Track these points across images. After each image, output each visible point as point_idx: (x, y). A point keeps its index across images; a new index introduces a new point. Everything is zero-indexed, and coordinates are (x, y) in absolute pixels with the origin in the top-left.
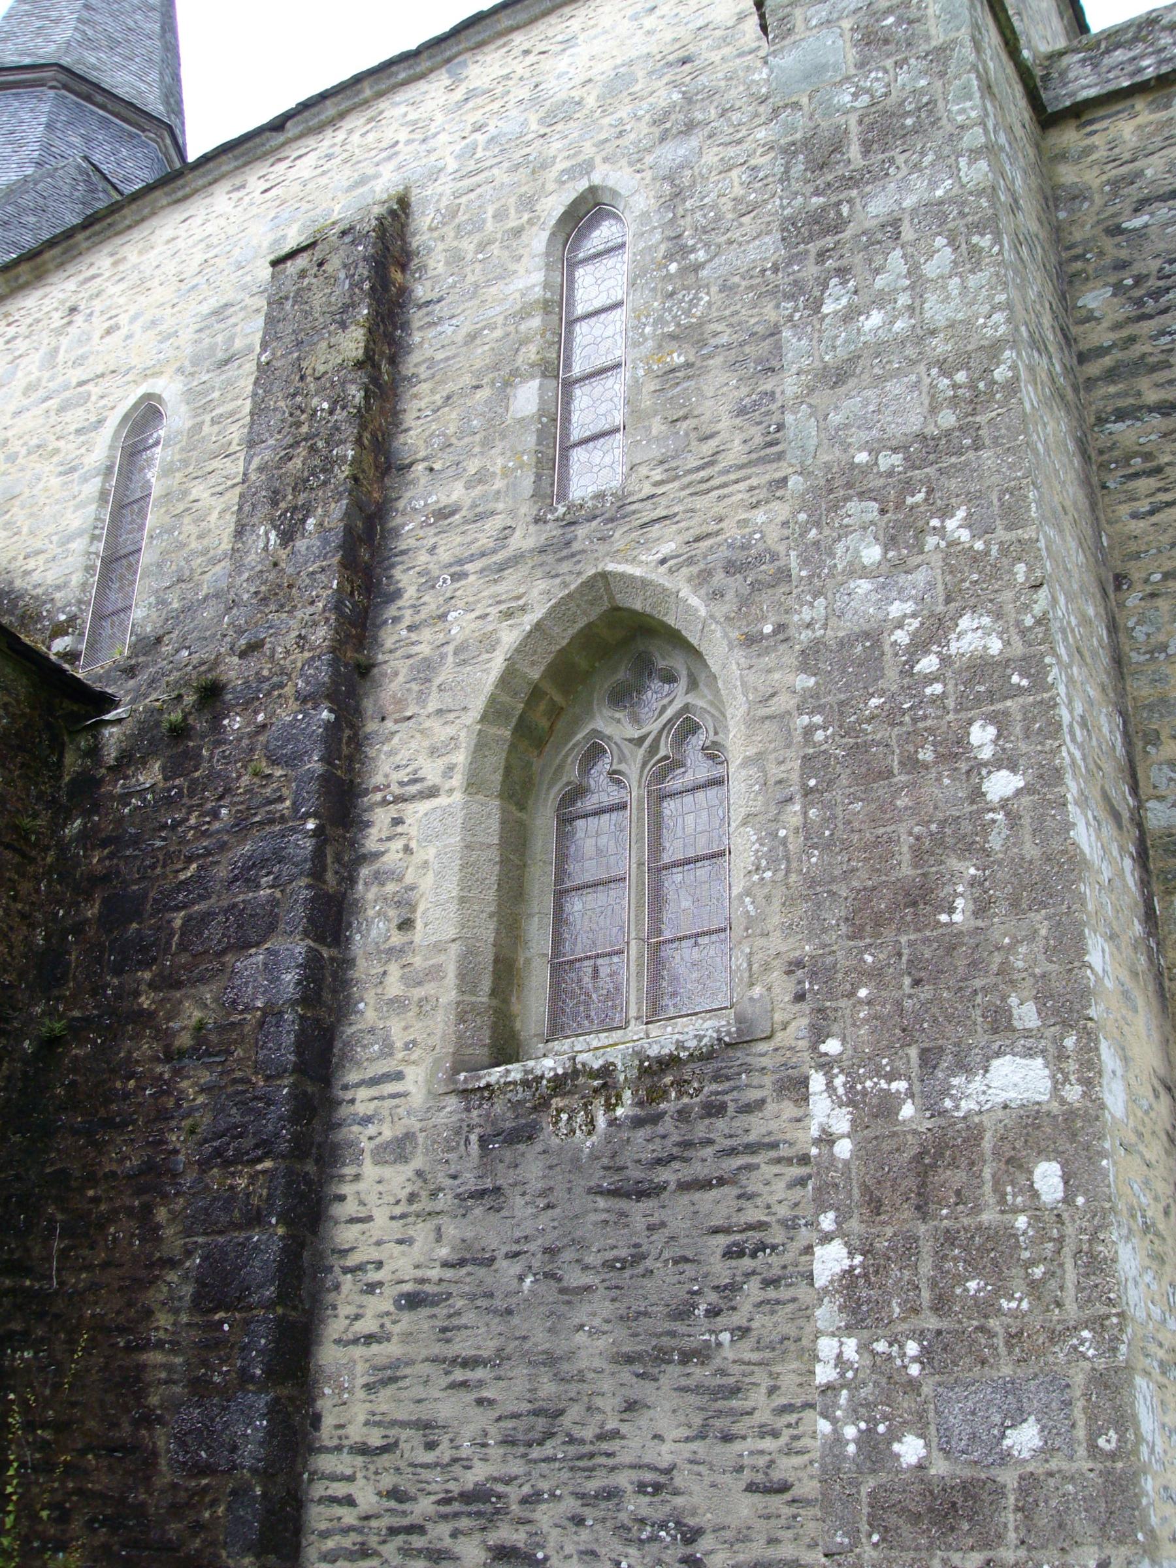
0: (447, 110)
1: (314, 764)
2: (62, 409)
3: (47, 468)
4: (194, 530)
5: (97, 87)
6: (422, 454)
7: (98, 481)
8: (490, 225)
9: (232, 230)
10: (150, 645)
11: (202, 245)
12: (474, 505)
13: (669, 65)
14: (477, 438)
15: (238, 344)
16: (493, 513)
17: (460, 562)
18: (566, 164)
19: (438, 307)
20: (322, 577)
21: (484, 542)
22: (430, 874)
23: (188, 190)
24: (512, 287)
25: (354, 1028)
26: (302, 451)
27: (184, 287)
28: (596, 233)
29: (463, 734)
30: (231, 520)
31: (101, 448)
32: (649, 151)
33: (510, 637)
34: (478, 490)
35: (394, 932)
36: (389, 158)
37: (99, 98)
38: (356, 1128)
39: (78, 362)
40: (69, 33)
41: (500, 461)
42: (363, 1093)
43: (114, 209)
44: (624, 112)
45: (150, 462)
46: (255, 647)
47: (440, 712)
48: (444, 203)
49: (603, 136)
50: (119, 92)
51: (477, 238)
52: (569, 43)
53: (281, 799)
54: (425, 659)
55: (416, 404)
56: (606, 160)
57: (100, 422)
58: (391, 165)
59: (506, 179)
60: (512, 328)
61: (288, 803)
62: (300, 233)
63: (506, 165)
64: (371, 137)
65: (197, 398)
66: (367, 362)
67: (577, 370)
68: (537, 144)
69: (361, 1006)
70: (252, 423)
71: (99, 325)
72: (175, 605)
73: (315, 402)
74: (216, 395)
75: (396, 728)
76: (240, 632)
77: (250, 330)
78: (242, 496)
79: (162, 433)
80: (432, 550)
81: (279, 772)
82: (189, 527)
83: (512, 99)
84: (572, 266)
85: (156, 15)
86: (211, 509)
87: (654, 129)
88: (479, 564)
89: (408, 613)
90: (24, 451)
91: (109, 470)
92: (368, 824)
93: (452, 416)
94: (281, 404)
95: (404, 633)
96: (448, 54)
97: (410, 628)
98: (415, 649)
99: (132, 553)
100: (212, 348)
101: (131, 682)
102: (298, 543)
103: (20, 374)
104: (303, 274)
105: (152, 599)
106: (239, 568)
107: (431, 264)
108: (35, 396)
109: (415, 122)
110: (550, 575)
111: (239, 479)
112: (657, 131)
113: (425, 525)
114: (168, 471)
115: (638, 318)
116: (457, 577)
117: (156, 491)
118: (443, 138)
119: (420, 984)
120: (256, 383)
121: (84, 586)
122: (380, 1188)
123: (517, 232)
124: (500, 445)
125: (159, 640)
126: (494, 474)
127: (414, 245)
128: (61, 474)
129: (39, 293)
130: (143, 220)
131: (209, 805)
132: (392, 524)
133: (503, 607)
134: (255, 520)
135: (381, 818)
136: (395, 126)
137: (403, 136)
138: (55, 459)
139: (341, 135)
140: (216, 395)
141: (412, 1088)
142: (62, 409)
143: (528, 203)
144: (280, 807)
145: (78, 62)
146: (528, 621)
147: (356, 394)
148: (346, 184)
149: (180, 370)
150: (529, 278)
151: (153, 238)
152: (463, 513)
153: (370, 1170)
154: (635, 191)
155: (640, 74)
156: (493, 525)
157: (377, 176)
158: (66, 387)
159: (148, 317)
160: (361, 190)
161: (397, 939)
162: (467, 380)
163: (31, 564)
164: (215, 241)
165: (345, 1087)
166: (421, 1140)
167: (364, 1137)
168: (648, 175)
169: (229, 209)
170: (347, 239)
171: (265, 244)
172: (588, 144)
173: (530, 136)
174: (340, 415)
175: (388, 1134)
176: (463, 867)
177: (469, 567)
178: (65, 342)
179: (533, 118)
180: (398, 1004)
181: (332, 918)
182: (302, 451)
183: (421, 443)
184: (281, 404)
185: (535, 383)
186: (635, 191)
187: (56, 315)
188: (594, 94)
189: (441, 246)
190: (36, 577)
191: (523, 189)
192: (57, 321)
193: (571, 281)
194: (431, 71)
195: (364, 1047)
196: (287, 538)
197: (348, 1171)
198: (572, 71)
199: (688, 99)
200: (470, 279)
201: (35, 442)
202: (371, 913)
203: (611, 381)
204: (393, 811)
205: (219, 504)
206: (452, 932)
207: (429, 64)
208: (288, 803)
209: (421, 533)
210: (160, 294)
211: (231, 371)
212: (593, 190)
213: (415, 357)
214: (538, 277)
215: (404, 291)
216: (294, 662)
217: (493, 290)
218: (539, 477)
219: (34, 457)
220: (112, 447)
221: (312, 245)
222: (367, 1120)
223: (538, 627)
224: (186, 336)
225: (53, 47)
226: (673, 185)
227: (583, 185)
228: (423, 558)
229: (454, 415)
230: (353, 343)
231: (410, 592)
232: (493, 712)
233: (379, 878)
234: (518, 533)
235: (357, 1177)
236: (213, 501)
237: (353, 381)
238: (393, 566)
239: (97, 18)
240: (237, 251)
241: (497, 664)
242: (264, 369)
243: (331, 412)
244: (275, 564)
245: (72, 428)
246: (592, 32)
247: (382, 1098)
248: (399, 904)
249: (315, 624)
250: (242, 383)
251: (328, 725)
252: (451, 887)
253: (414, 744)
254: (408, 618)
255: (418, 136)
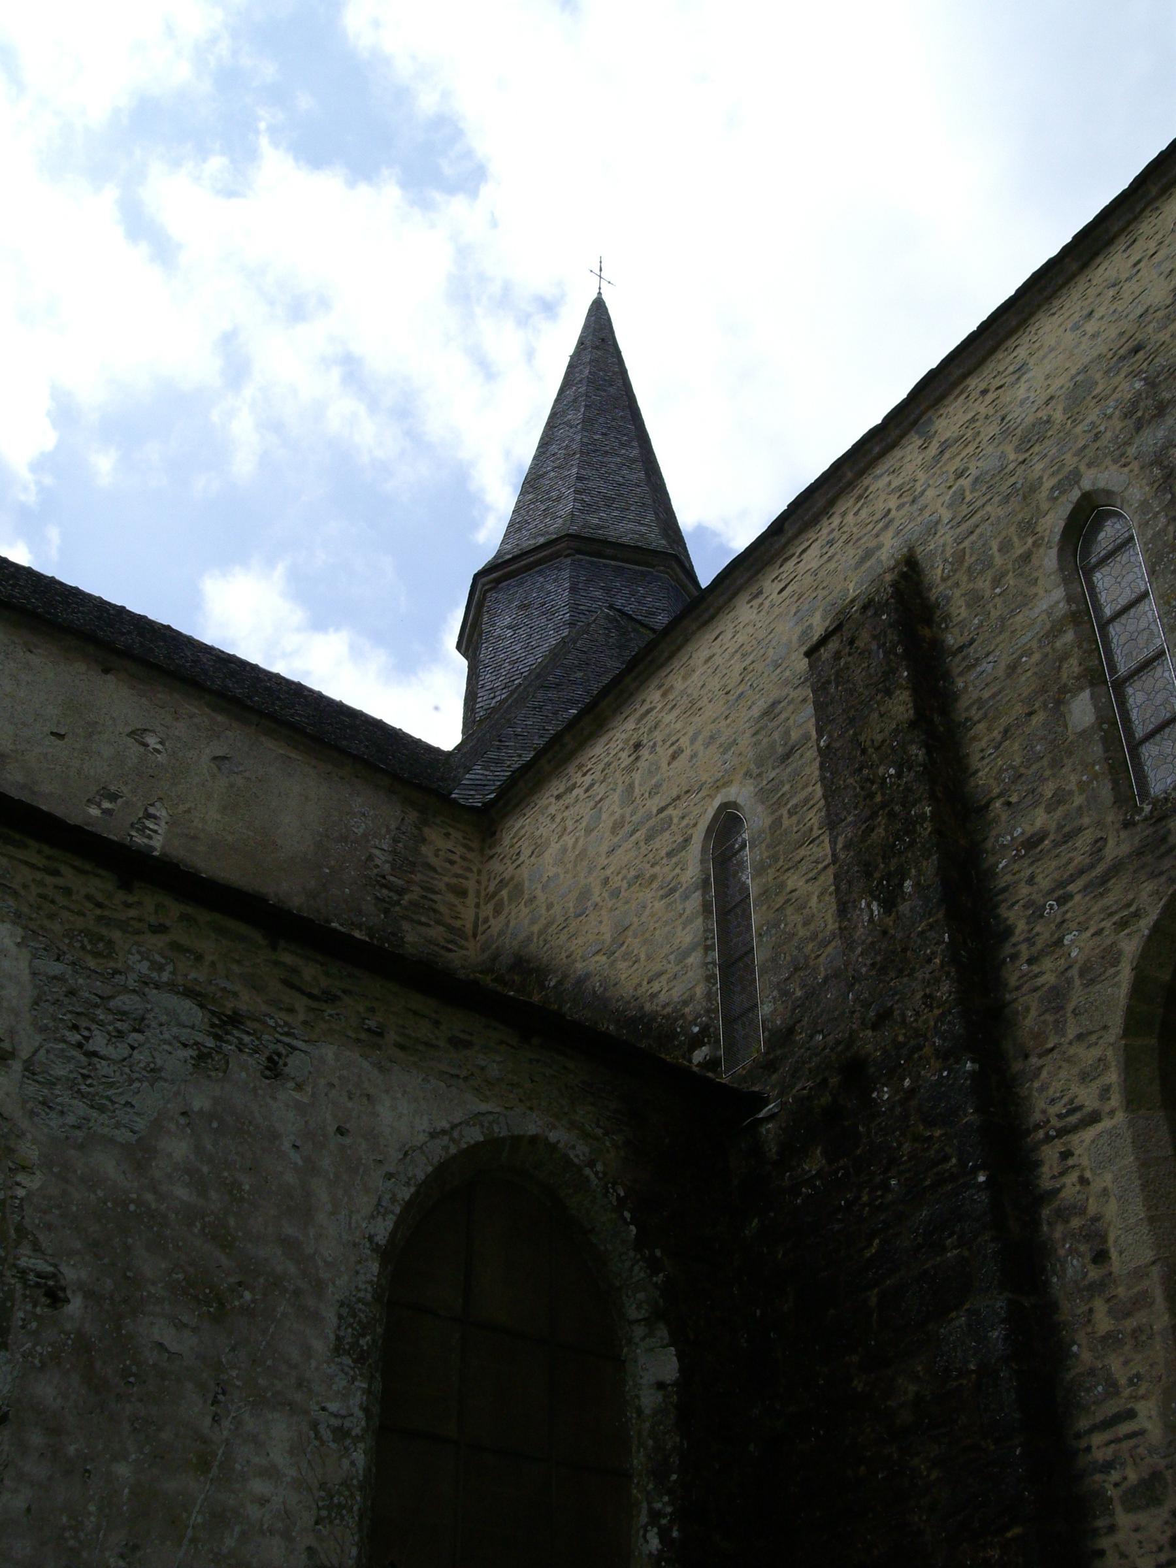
0: (927, 467)
1: (970, 1116)
2: (649, 839)
3: (647, 895)
4: (798, 919)
5: (605, 542)
6: (996, 791)
7: (698, 894)
8: (998, 560)
9: (761, 634)
10: (782, 1037)
11: (738, 655)
12: (1060, 827)
13: (1123, 358)
14: (1045, 762)
15: (795, 735)
16: (1080, 829)
17: (1062, 884)
18: (1054, 481)
19: (971, 650)
20: (931, 934)
21: (1079, 859)
22: (1113, 1200)
23: (712, 611)
24: (1037, 611)
25: (1073, 1373)
26: (881, 819)
27: (731, 697)
28: (1102, 535)
29: (1109, 1053)
30: (831, 902)
31: (692, 866)
32: (1128, 443)
33: (1130, 946)
34: (1060, 812)
35: (1091, 1267)
36: (886, 527)
37: (609, 551)
38: (1098, 1477)
39: (654, 791)
40: (571, 506)
41: (1073, 778)
42: (1097, 1439)
43: (651, 647)
44: (1093, 416)
45: (741, 865)
46: (884, 1016)
47: (1080, 1037)
48: (949, 552)
49: (1081, 443)
50: (624, 540)
51: (989, 574)
52: (1021, 370)
53: (946, 1159)
54: (1053, 988)
55: (977, 746)
56: (1089, 465)
57: (687, 841)
58: (890, 533)
59: (1001, 512)
60: (1048, 649)
61: (954, 1160)
62: (824, 619)
63: (997, 499)
64: (864, 513)
65: (768, 795)
66: (920, 721)
67: (1122, 670)
68: (1019, 471)
69: (1075, 1348)
70: (828, 805)
71: (664, 753)
72: (799, 993)
73: (881, 770)
74: (787, 787)
75: (1041, 1062)
76: (867, 1005)
77: (803, 721)
78: (836, 876)
79: (746, 836)
80: (1031, 881)
81: (938, 1133)
82: (793, 918)
83: (984, 438)
84: (1089, 572)
85: (638, 466)
86: (809, 895)
87: (1128, 422)
88: (1081, 882)
89: (1023, 947)
90: (625, 885)
91: (705, 883)
92: (1038, 1164)
93: (1014, 746)
94: (850, 781)
95: (1025, 967)
96: (912, 417)
97: (1030, 961)
98: (1040, 981)
99: (746, 953)
100: (772, 746)
101: (775, 1077)
102: (901, 908)
103: (604, 816)
104: (837, 656)
105: (775, 993)
106: (850, 946)
107: (954, 611)
108: (622, 833)
109: (900, 488)
110: (1153, 876)
111: (829, 860)
112: (1130, 423)
113: (1018, 858)
114: (760, 870)
115: (1168, 603)
116: (1063, 900)
117: (753, 891)
118: (930, 493)
119: (1128, 1315)
120: (822, 767)
121: (709, 996)
122: (1139, 1536)
123: (1026, 558)
124: (1069, 762)
125: (791, 1031)
126: (1071, 793)
127: (933, 598)
128: (662, 897)
129: (604, 740)
130: (679, 649)
131: (878, 1179)
132: (985, 866)
133: (1116, 918)
134: (855, 895)
135: (1049, 1154)
136: (883, 496)
137: (893, 503)
138: (655, 885)
139: (836, 521)
140: (787, 787)
141: (1148, 1425)
142: (649, 839)
143: (1028, 527)
144: (947, 1166)
145: (584, 527)
146: (1145, 925)
147: (917, 752)
148: (853, 562)
149: (748, 774)
150: (1050, 597)
151: (692, 662)
152: (1051, 837)
153: (1123, 1519)
154: (1126, 484)
155: (1098, 376)
156: (1083, 842)
157: (879, 547)
158: (649, 817)
159: (706, 733)
160: (869, 564)
161: (1094, 1274)
162: (1019, 709)
163: (656, 986)
164: (748, 648)
165: (1078, 1436)
166: (1169, 1478)
167: (1110, 1484)
168: (1135, 466)
169: (753, 617)
170: (870, 613)
171: (795, 638)
172: (1068, 456)
173: (1011, 467)
174: (908, 776)
175: (1133, 1477)
176: (1144, 1187)
177: (1071, 888)
178: (637, 776)
179: (1010, 450)
180: (1111, 1340)
181: (1025, 1264)
182: (881, 819)
183: (991, 781)
184: (850, 781)
185: (1086, 694)
186: (1126, 484)
187: (624, 755)
188: (1060, 408)
189: (957, 593)
190: (663, 997)
191: (1020, 516)
192: (625, 759)
193: (1092, 588)
194: (902, 437)
195: (1088, 1390)
196: (889, 905)
197: (1101, 1523)
198: (1032, 395)
199: (1151, 383)
200: (995, 614)
201: (633, 873)
202: (1062, 1252)
203: (1159, 670)
204: (1059, 1146)
205: (815, 888)
206: (1148, 1255)
207: (897, 432)
208: (954, 1160)
209: (1016, 867)
210: (710, 711)
211: (795, 762)
212: (1086, 496)
213: (964, 702)
214: (1059, 593)
215: (937, 644)
216: (926, 1022)
217: (1019, 618)
218: (1115, 782)
219: (635, 888)
220: (702, 861)
221: (838, 628)
222: (1108, 1466)
223: (1156, 928)
224: (745, 741)
225: (560, 521)
226: (1163, 468)
227: (1076, 494)
228: (1024, 890)
229: (1016, 746)
230: (901, 706)
231: (1021, 926)
232: (1134, 1024)
233: (1063, 1215)
234: (1111, 843)
235: (1112, 1529)
236: (810, 887)
237: (912, 742)
238: (996, 906)
239: (591, 484)
240: (771, 652)
241: (1126, 973)
242: (825, 754)
243: (899, 775)
244: (885, 933)
245: (663, 853)
246: (1041, 353)
247: (1118, 1440)
248: (1088, 1238)
249: (938, 981)
250: (808, 771)
251: (972, 1075)
252: (1138, 1209)
253: (1063, 1074)
254: (1025, 951)
255: (907, 499)
